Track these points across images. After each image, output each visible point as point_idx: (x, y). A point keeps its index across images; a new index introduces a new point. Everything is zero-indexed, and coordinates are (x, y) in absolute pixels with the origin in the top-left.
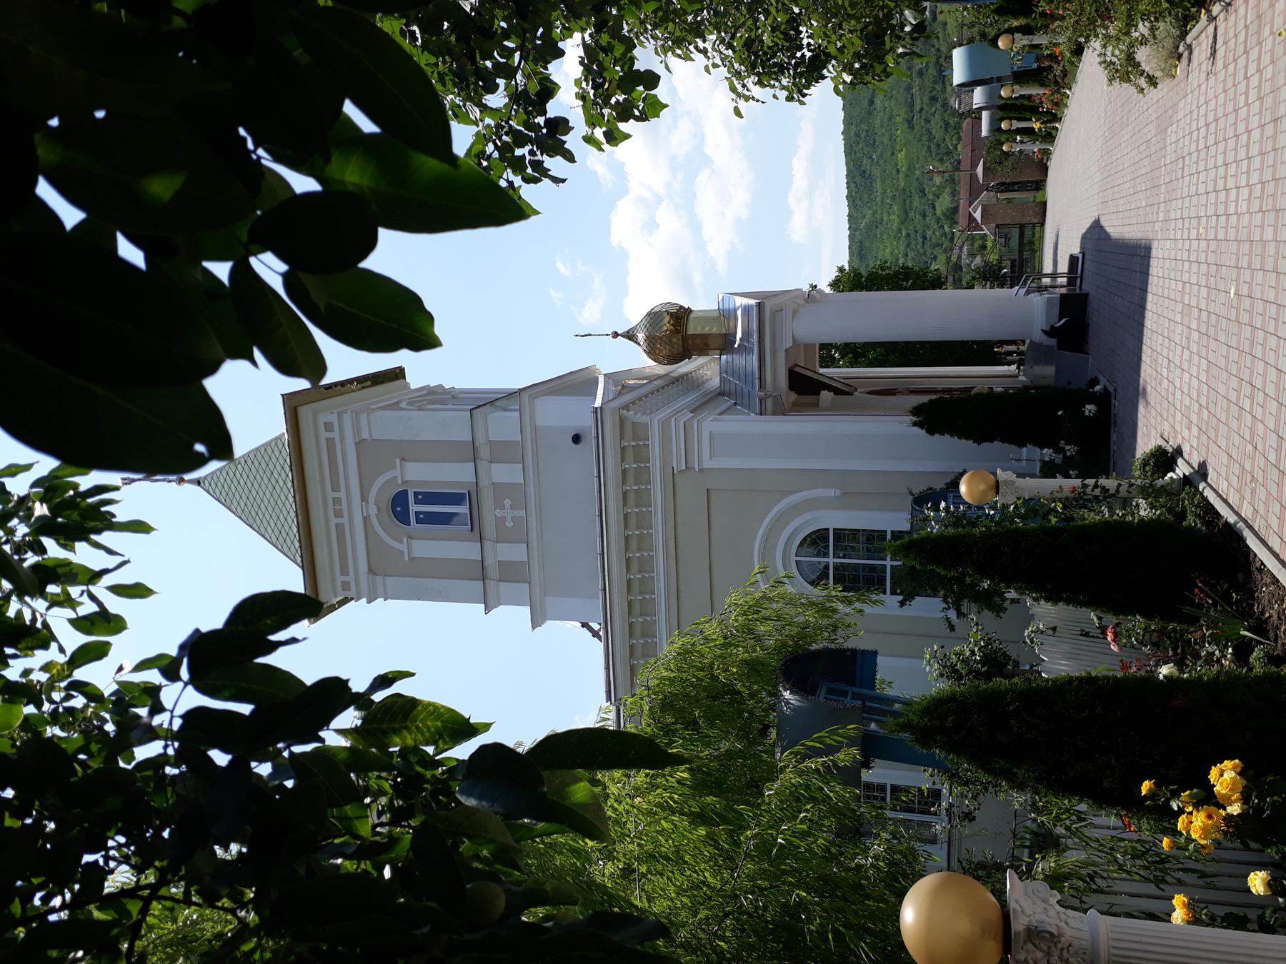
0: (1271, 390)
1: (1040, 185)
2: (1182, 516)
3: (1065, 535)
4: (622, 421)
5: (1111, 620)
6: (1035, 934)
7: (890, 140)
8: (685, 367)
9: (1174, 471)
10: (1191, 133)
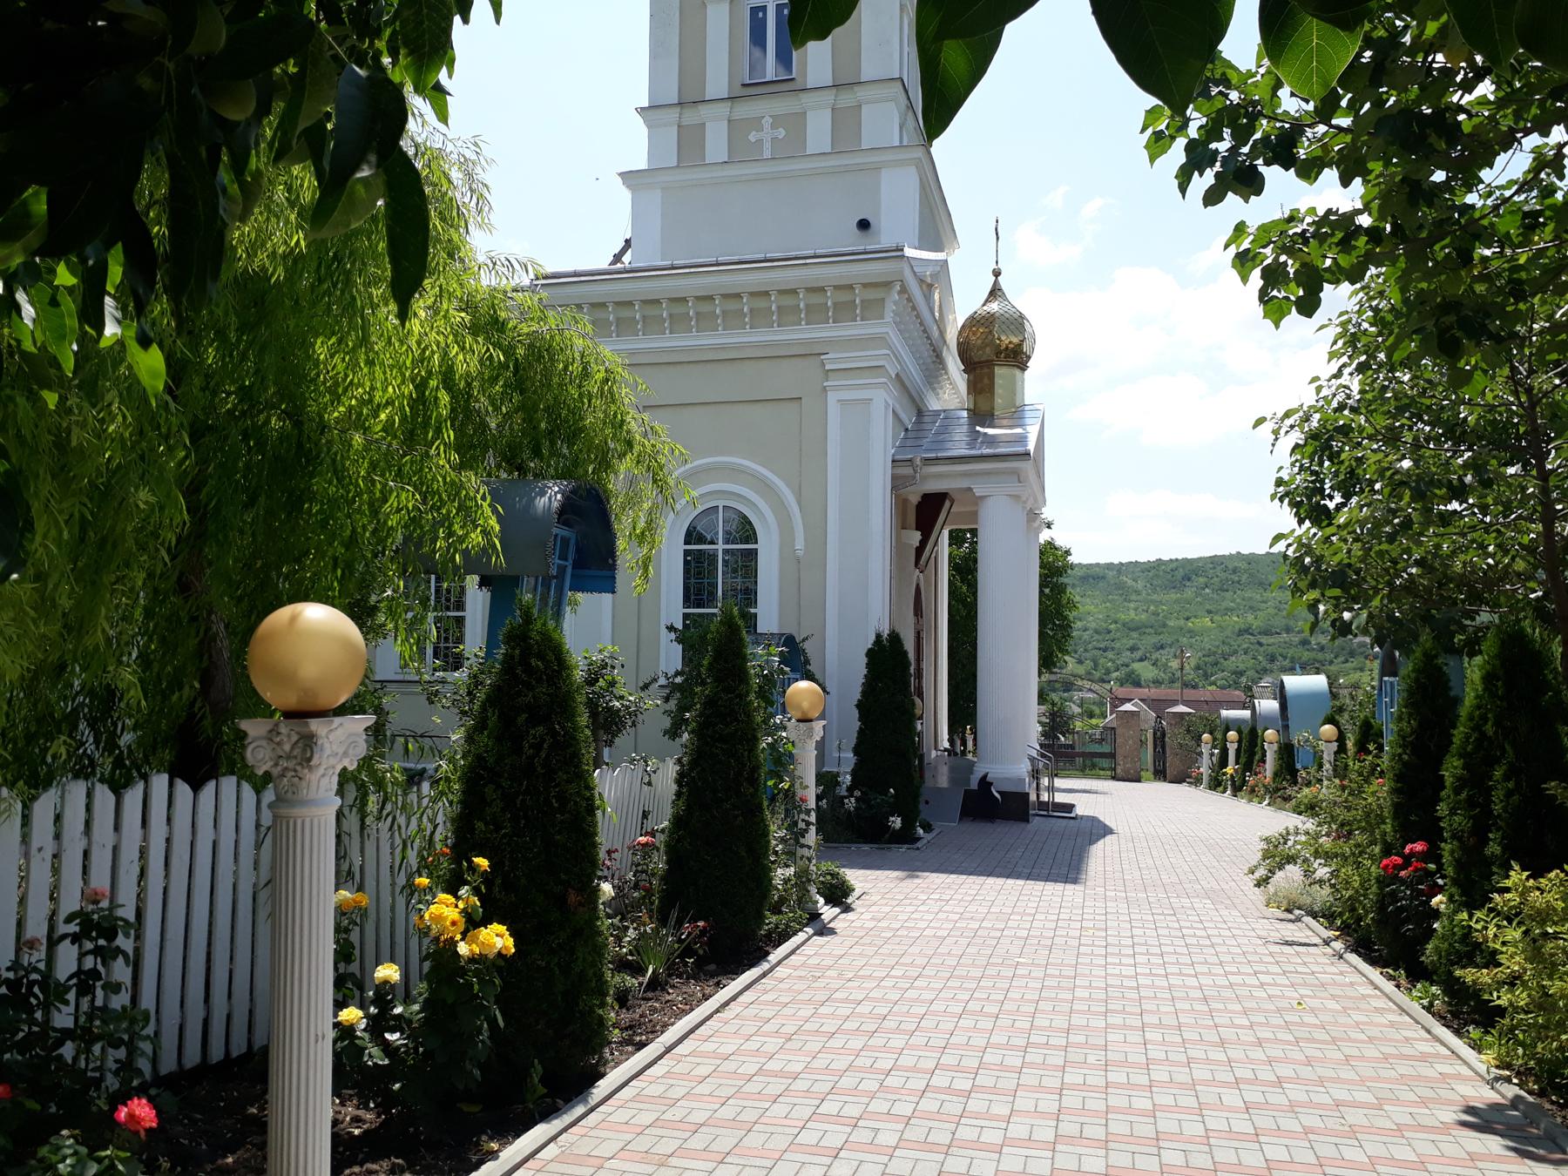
0: (911, 994)
1: (1161, 774)
2: (776, 910)
3: (751, 790)
4: (887, 285)
5: (661, 839)
6: (308, 742)
7: (1227, 609)
8: (954, 365)
9: (826, 903)
10: (1201, 922)
